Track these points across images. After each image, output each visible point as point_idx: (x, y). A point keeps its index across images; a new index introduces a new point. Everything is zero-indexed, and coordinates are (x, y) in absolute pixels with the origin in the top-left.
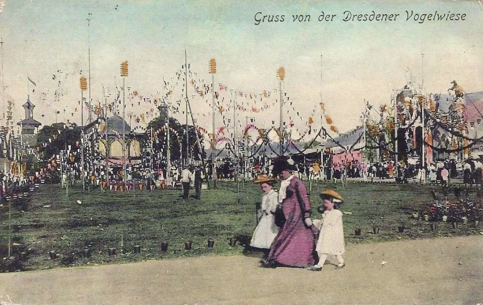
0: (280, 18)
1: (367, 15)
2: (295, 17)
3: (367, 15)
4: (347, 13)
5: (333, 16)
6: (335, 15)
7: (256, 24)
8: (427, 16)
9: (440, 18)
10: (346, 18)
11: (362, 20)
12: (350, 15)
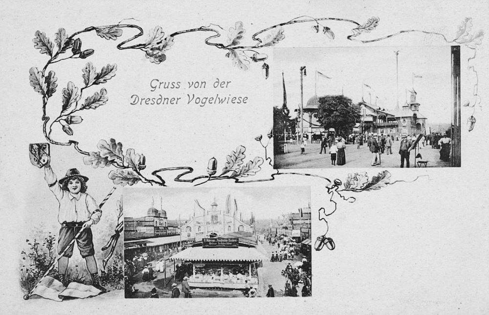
0: (171, 85)
1: (154, 99)
2: (191, 84)
3: (154, 99)
4: (135, 97)
5: (228, 83)
6: (230, 82)
7: (152, 91)
8: (208, 99)
9: (221, 101)
10: (134, 102)
11: (236, 103)
12: (137, 99)
